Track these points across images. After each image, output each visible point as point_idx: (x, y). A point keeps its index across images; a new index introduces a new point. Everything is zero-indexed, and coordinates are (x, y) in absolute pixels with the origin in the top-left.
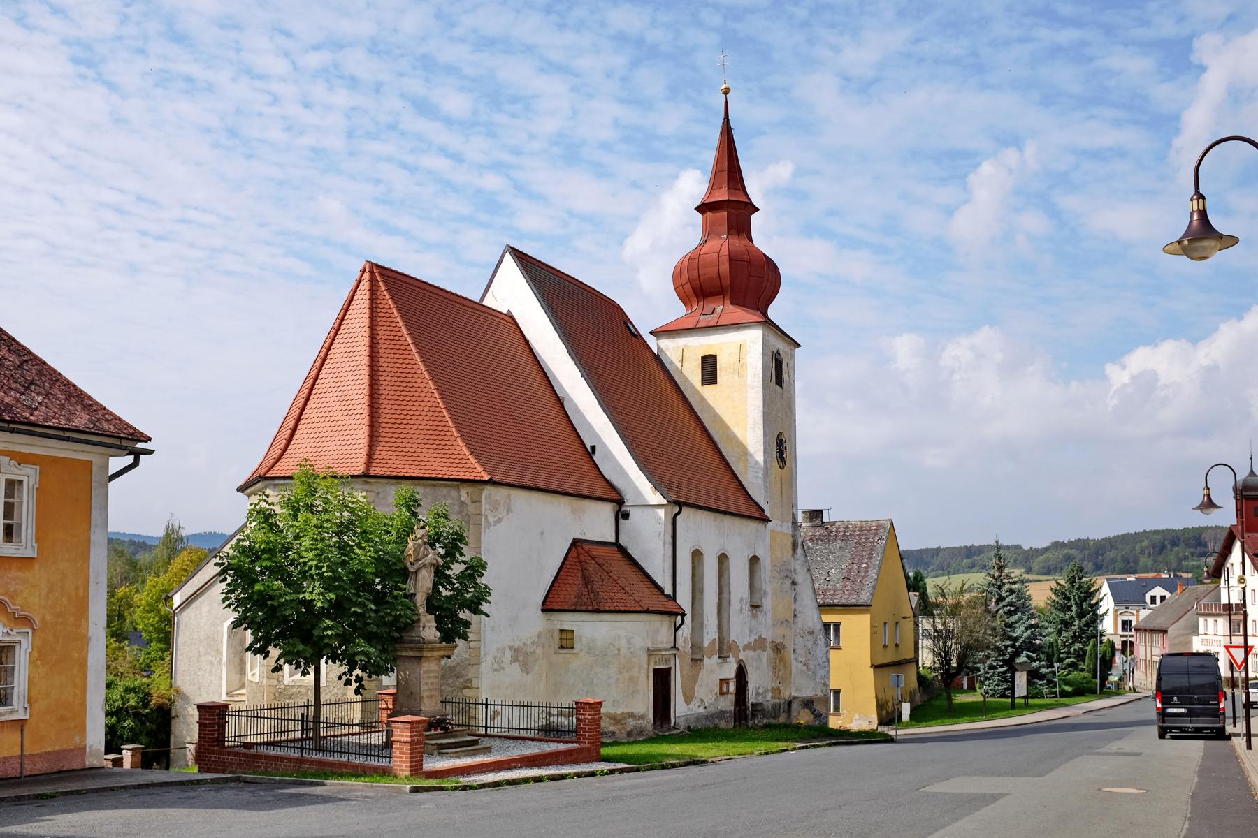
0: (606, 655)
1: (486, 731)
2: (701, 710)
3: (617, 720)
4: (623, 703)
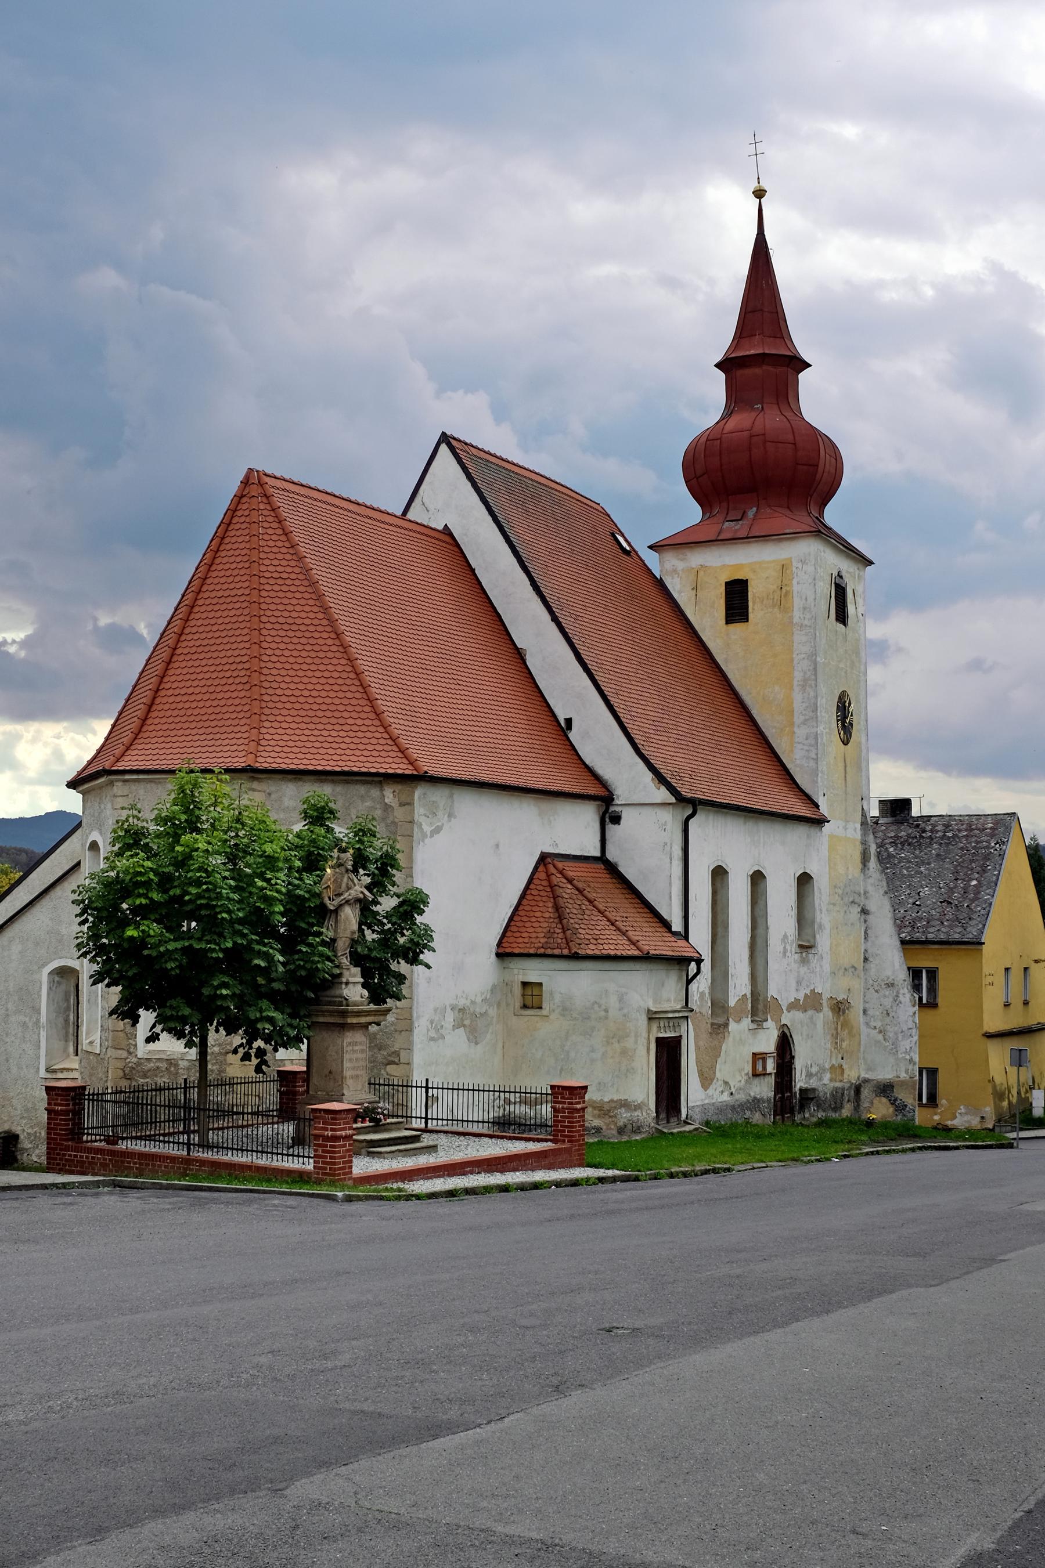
0: (589, 1018)
1: (426, 1123)
2: (725, 1097)
3: (605, 1110)
4: (613, 1085)
